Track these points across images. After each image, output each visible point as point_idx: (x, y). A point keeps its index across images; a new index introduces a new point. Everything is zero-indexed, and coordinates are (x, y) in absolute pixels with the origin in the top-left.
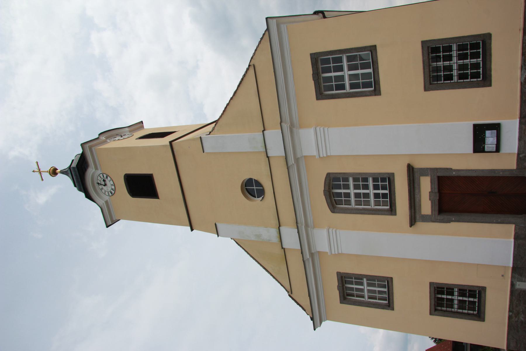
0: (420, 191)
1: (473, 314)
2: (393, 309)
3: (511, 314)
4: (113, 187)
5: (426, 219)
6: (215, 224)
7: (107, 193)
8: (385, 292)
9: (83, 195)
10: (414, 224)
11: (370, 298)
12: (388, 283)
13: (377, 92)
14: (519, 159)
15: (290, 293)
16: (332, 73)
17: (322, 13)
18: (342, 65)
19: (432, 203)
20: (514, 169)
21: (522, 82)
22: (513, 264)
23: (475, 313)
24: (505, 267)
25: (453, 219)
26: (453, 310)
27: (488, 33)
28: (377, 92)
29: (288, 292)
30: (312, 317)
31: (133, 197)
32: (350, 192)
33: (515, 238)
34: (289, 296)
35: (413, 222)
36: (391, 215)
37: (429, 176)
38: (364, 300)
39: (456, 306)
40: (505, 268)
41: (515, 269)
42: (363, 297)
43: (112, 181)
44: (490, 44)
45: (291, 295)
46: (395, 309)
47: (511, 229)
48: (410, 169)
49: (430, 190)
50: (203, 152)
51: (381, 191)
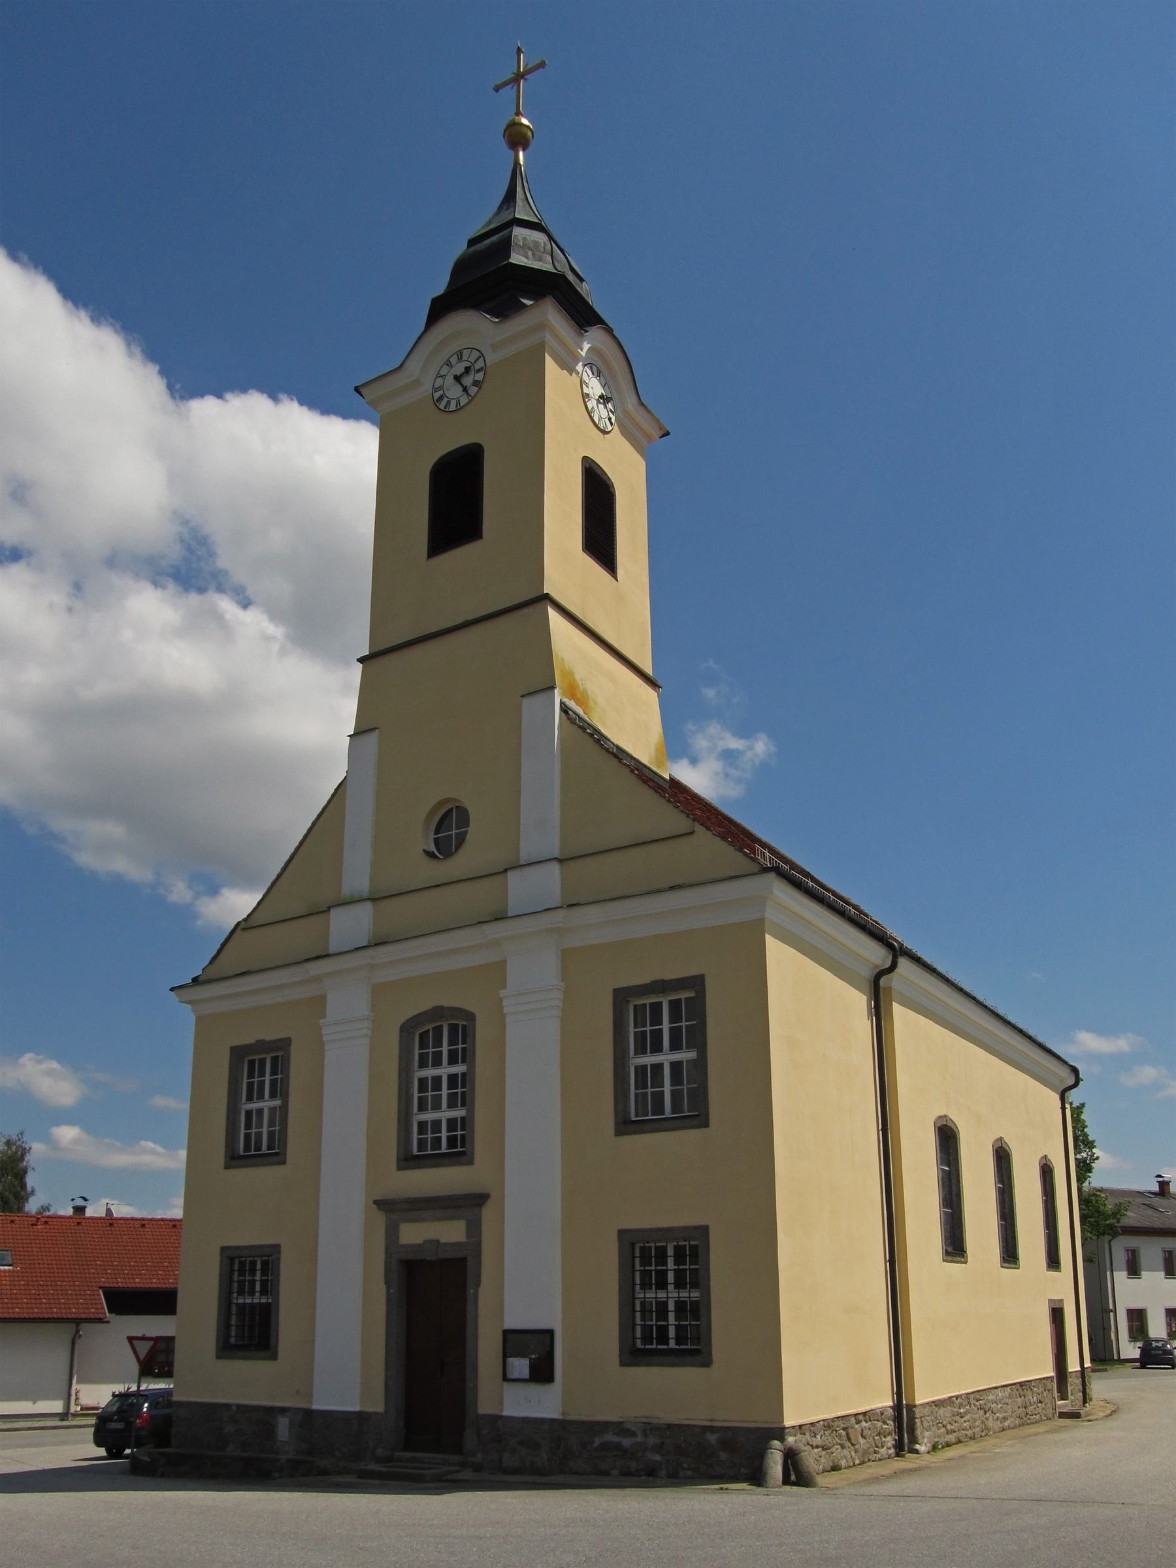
0: (440, 1219)
1: (229, 1336)
2: (227, 1167)
3: (234, 1408)
4: (453, 407)
5: (392, 1232)
6: (374, 729)
7: (439, 382)
8: (258, 1148)
9: (440, 287)
10: (379, 1209)
11: (249, 1114)
12: (275, 1154)
13: (625, 1125)
14: (495, 1419)
15: (243, 925)
16: (668, 1023)
17: (880, 978)
18: (682, 1049)
19: (419, 1245)
20: (477, 1410)
21: (624, 1425)
22: (318, 1411)
23: (639, 1344)
24: (311, 1395)
25: (392, 1291)
26: (235, 1295)
27: (712, 1361)
28: (625, 1125)
29: (245, 920)
30: (200, 979)
31: (431, 473)
32: (444, 1065)
33: (360, 1415)
34: (238, 924)
35: (384, 1205)
36: (399, 1160)
37: (468, 1240)
38: (241, 1101)
39: (241, 1301)
40: (310, 1395)
41: (309, 1413)
42: (250, 1098)
43: (468, 401)
44: (693, 1365)
45: (238, 931)
46: (227, 1171)
47: (377, 1406)
48: (478, 1200)
49: (443, 1240)
50: (522, 694)
51: (444, 1134)
